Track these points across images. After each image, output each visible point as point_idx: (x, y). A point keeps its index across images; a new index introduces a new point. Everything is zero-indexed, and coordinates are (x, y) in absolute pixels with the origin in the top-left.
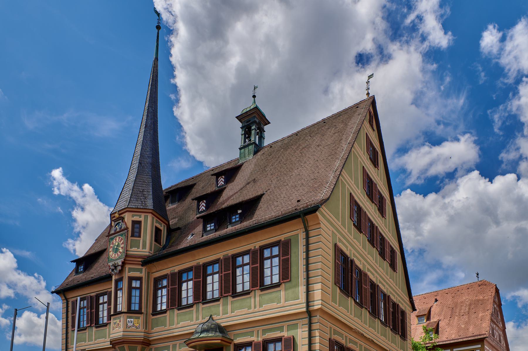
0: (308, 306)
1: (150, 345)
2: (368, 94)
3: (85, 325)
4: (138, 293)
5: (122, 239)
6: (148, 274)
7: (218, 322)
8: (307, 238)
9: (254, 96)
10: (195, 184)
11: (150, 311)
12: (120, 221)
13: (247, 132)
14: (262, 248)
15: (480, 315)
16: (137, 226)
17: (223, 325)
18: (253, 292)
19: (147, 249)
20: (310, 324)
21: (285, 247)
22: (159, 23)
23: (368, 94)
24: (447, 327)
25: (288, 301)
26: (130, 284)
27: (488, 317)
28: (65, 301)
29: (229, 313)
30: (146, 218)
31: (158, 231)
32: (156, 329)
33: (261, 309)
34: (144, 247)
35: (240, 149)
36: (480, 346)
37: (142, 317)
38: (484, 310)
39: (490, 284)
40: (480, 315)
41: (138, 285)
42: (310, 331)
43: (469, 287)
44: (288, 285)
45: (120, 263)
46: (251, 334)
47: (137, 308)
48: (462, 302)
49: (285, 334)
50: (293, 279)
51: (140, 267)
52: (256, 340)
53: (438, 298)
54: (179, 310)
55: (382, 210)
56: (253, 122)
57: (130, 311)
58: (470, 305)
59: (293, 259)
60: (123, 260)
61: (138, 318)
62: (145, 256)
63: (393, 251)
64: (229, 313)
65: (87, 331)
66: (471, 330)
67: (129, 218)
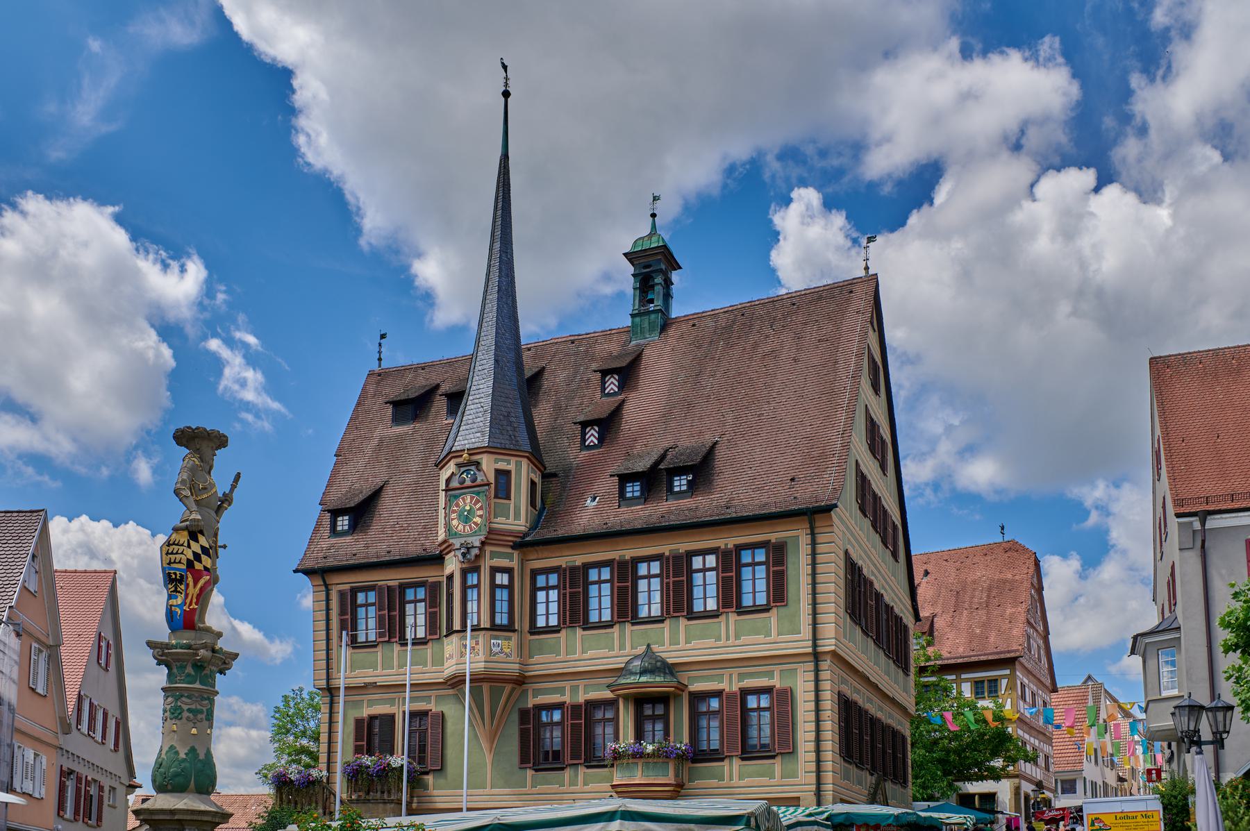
0: (815, 645)
1: (524, 683)
2: (867, 268)
3: (372, 637)
4: (505, 593)
5: (478, 501)
6: (522, 562)
7: (663, 655)
8: (814, 543)
9: (653, 215)
10: (542, 370)
11: (527, 626)
12: (473, 468)
13: (645, 284)
14: (739, 548)
15: (1009, 611)
16: (502, 480)
17: (670, 661)
18: (724, 616)
19: (522, 521)
20: (817, 671)
21: (778, 553)
22: (506, 85)
23: (867, 268)
24: (948, 630)
25: (780, 635)
26: (493, 578)
27: (1022, 618)
28: (323, 588)
29: (680, 643)
30: (518, 465)
31: (533, 483)
32: (536, 658)
33: (737, 642)
34: (517, 516)
35: (633, 316)
36: (1008, 672)
37: (514, 636)
38: (1016, 603)
39: (1025, 550)
40: (1009, 611)
41: (506, 582)
42: (817, 680)
43: (988, 550)
44: (782, 610)
45: (477, 544)
46: (720, 678)
47: (505, 622)
48: (974, 582)
49: (776, 682)
50: (790, 602)
51: (510, 550)
52: (727, 690)
53: (930, 568)
54: (584, 629)
55: (883, 467)
56: (653, 268)
57: (494, 627)
58: (990, 589)
59: (791, 572)
60: (482, 538)
61: (509, 639)
62: (520, 532)
63: (895, 527)
64: (680, 643)
65: (379, 648)
66: (992, 639)
67: (489, 465)
